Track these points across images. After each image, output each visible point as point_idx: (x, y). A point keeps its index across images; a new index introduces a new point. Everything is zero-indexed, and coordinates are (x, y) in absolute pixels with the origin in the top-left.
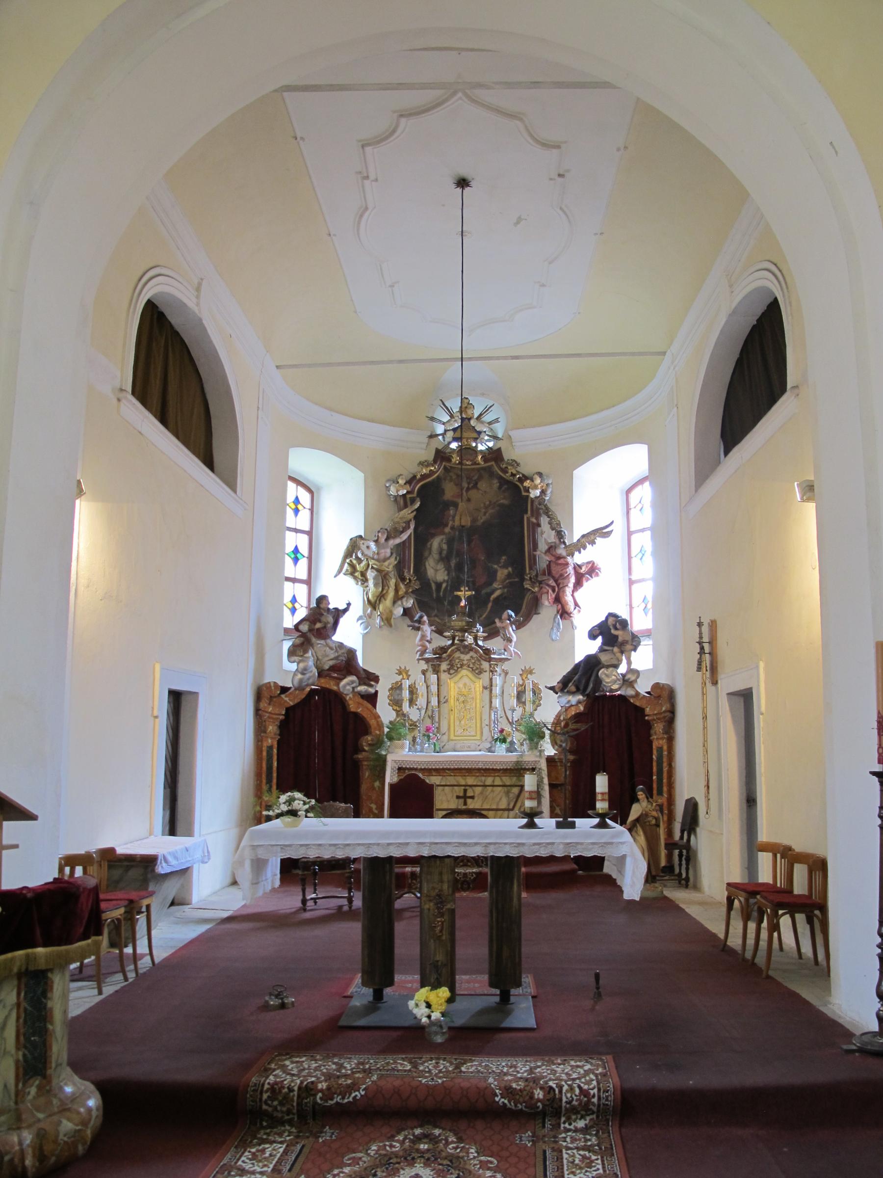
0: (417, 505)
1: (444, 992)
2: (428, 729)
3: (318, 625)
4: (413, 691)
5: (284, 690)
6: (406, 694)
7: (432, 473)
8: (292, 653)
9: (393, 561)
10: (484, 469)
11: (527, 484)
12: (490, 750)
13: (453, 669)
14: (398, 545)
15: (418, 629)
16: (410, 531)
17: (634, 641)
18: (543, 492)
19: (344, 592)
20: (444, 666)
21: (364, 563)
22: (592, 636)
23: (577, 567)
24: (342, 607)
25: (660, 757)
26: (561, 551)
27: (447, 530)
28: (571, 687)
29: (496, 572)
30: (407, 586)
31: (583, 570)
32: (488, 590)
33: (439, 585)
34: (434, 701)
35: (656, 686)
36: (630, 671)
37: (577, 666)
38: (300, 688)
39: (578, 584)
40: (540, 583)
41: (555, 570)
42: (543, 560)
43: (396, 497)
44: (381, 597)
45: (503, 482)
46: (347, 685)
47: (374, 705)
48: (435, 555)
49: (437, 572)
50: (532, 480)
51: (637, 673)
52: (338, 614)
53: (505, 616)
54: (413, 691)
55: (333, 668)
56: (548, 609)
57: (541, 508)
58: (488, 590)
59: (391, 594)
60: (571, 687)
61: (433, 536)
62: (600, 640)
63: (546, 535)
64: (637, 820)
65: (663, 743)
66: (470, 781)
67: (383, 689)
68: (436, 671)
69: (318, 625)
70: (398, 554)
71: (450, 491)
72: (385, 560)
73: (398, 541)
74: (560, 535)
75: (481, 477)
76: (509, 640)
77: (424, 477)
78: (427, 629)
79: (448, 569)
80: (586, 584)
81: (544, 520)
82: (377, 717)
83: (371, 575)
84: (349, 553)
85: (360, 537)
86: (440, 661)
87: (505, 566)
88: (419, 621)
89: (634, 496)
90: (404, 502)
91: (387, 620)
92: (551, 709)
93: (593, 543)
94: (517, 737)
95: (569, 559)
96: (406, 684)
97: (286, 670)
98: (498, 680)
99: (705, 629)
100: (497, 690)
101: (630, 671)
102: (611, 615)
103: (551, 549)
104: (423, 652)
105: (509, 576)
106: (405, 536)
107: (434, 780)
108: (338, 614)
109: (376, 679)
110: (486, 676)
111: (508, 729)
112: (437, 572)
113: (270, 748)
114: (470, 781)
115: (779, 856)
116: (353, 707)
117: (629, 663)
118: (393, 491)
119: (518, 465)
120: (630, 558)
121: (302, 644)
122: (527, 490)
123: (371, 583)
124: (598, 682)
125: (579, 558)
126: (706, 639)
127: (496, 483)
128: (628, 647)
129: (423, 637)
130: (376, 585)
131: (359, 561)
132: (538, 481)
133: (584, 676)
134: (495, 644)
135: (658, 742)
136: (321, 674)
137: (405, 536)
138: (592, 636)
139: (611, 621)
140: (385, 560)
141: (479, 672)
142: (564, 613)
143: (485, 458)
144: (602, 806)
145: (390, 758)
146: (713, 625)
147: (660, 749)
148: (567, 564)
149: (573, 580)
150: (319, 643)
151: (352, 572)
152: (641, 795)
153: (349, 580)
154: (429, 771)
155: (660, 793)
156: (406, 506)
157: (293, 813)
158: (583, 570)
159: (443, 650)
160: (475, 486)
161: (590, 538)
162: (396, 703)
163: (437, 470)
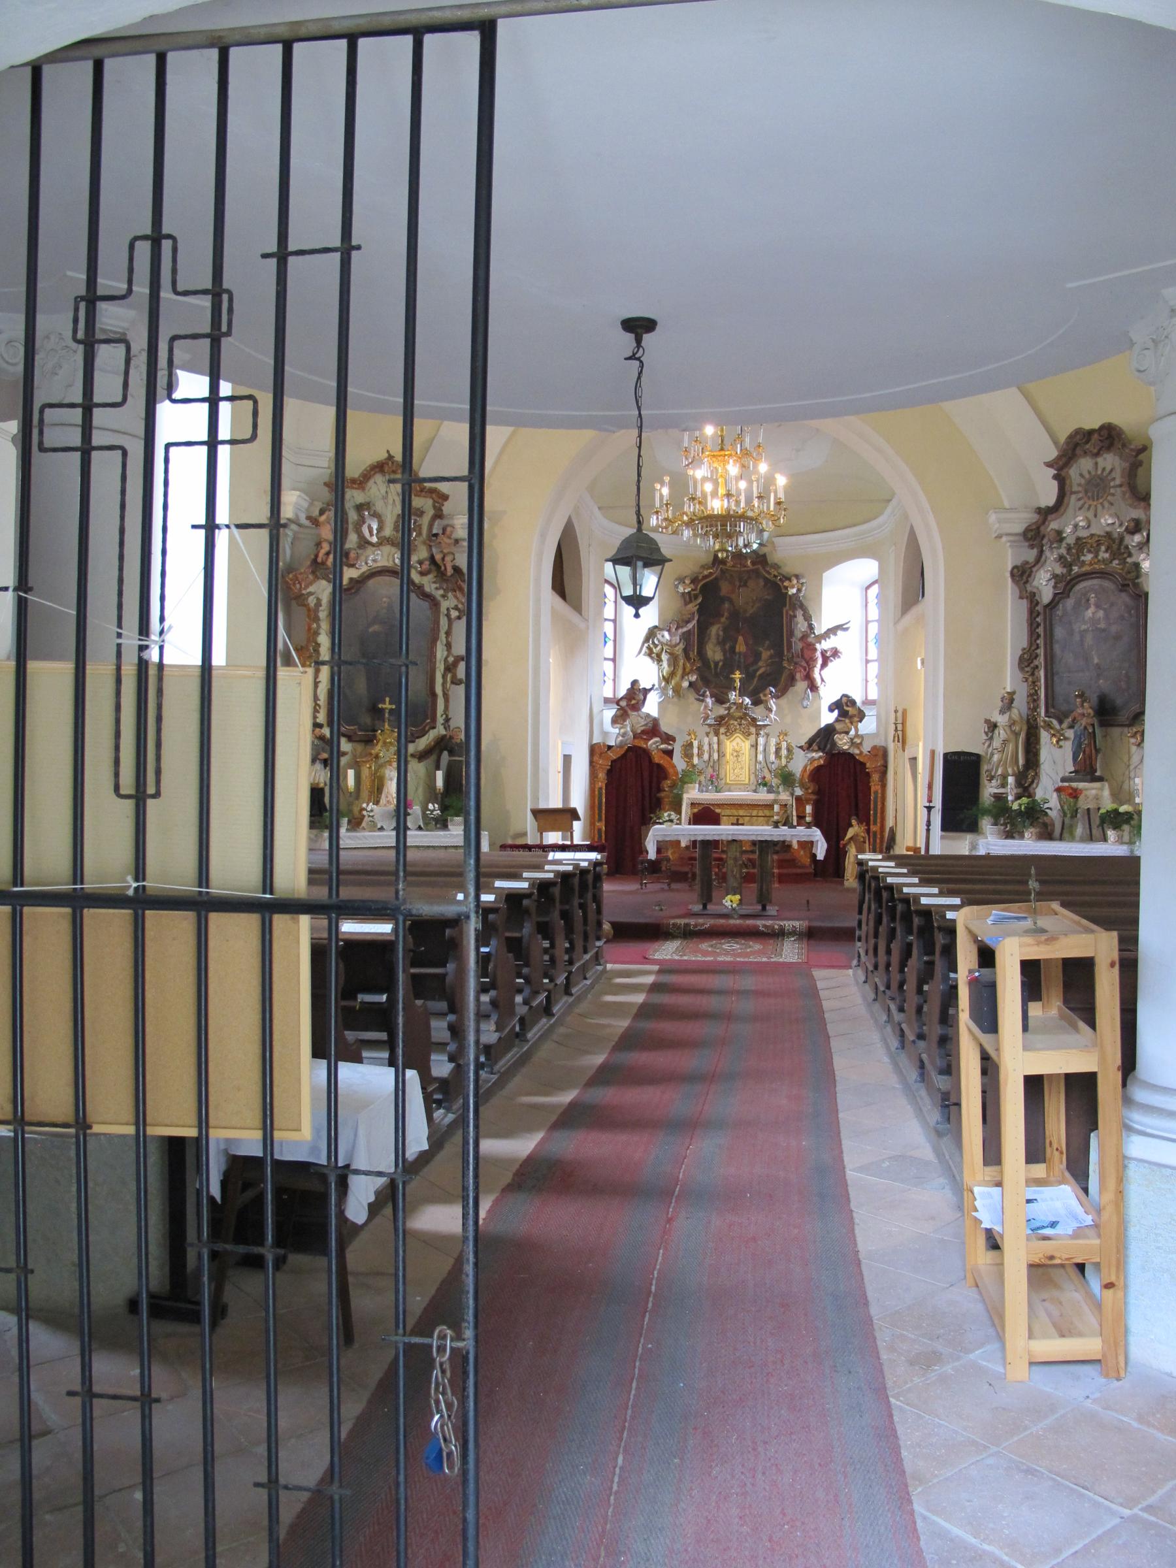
0: (700, 600)
1: (738, 897)
2: (712, 776)
3: (633, 702)
4: (700, 748)
5: (610, 747)
6: (695, 751)
7: (711, 574)
8: (615, 721)
9: (682, 646)
10: (752, 571)
11: (786, 584)
12: (755, 791)
13: (729, 733)
14: (684, 633)
15: (703, 701)
16: (695, 622)
17: (861, 716)
18: (799, 590)
19: (648, 673)
20: (722, 730)
21: (659, 648)
22: (831, 710)
23: (823, 653)
24: (648, 687)
25: (876, 798)
26: (811, 639)
27: (723, 620)
28: (815, 746)
29: (760, 653)
30: (692, 664)
31: (828, 654)
32: (755, 667)
33: (716, 664)
34: (716, 756)
35: (874, 748)
36: (857, 735)
37: (821, 730)
38: (620, 746)
39: (824, 665)
40: (796, 663)
41: (807, 653)
42: (798, 646)
43: (683, 594)
44: (672, 674)
45: (767, 580)
46: (653, 744)
47: (672, 758)
48: (713, 639)
49: (714, 653)
50: (790, 580)
51: (862, 737)
52: (646, 692)
53: (767, 691)
54: (700, 748)
55: (643, 732)
56: (801, 685)
57: (797, 604)
58: (755, 667)
59: (680, 672)
60: (815, 746)
61: (712, 624)
62: (836, 712)
63: (801, 626)
64: (851, 838)
65: (878, 788)
66: (741, 813)
67: (678, 749)
68: (717, 734)
69: (633, 702)
70: (686, 640)
71: (725, 588)
72: (676, 646)
73: (685, 629)
74: (811, 627)
75: (749, 578)
76: (770, 710)
77: (705, 577)
78: (709, 701)
79: (724, 652)
80: (830, 664)
81: (799, 613)
82: (674, 767)
83: (664, 657)
84: (647, 640)
85: (656, 627)
86: (721, 725)
87: (768, 649)
88: (703, 695)
89: (869, 591)
90: (688, 598)
91: (677, 691)
92: (801, 763)
93: (835, 634)
94: (775, 782)
95: (818, 646)
96: (695, 744)
97: (613, 735)
98: (761, 740)
99: (899, 714)
100: (761, 748)
101: (857, 735)
102: (844, 696)
103: (804, 637)
104: (706, 718)
105: (771, 657)
106: (690, 626)
107: (718, 811)
108: (646, 692)
109: (674, 739)
110: (753, 737)
111: (768, 776)
112: (714, 653)
113: (601, 789)
114: (741, 813)
115: (923, 852)
116: (656, 760)
117: (857, 730)
118: (681, 589)
119: (779, 567)
120: (867, 642)
121: (622, 715)
122: (786, 588)
123: (665, 664)
124: (834, 744)
125: (825, 645)
126: (900, 721)
127: (762, 583)
128: (856, 719)
129: (706, 707)
130: (669, 665)
131: (656, 646)
132: (795, 582)
133: (825, 736)
134: (758, 712)
135: (875, 787)
136: (635, 736)
137: (690, 626)
138: (831, 710)
139: (844, 700)
140: (676, 646)
141: (747, 735)
142: (813, 687)
143: (753, 563)
144: (808, 819)
145: (685, 796)
146: (905, 712)
147: (876, 792)
148: (816, 650)
149: (820, 661)
150: (633, 714)
151: (650, 653)
152: (854, 822)
153: (648, 659)
154: (719, 805)
155: (875, 823)
156: (691, 601)
157: (671, 821)
158: (828, 654)
159: (722, 718)
160: (745, 585)
161: (833, 631)
162: (688, 755)
163: (715, 572)
